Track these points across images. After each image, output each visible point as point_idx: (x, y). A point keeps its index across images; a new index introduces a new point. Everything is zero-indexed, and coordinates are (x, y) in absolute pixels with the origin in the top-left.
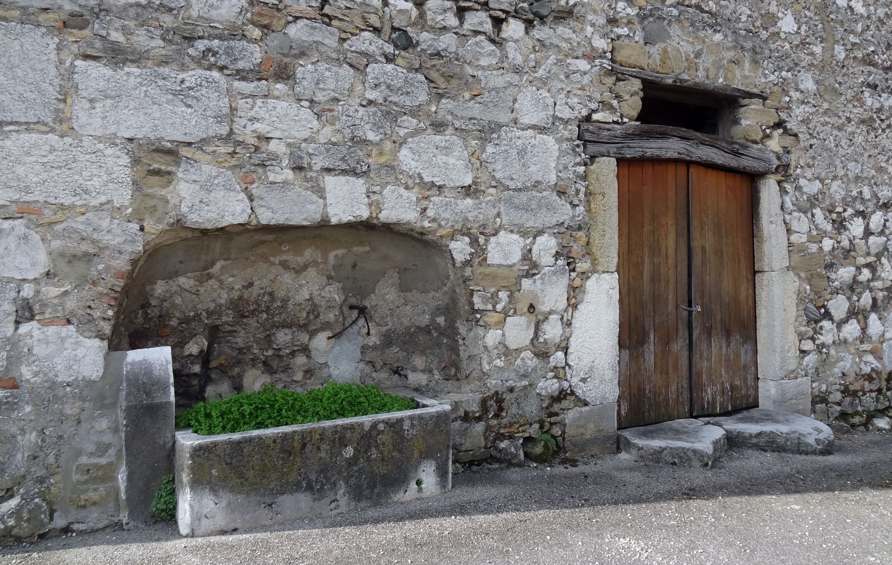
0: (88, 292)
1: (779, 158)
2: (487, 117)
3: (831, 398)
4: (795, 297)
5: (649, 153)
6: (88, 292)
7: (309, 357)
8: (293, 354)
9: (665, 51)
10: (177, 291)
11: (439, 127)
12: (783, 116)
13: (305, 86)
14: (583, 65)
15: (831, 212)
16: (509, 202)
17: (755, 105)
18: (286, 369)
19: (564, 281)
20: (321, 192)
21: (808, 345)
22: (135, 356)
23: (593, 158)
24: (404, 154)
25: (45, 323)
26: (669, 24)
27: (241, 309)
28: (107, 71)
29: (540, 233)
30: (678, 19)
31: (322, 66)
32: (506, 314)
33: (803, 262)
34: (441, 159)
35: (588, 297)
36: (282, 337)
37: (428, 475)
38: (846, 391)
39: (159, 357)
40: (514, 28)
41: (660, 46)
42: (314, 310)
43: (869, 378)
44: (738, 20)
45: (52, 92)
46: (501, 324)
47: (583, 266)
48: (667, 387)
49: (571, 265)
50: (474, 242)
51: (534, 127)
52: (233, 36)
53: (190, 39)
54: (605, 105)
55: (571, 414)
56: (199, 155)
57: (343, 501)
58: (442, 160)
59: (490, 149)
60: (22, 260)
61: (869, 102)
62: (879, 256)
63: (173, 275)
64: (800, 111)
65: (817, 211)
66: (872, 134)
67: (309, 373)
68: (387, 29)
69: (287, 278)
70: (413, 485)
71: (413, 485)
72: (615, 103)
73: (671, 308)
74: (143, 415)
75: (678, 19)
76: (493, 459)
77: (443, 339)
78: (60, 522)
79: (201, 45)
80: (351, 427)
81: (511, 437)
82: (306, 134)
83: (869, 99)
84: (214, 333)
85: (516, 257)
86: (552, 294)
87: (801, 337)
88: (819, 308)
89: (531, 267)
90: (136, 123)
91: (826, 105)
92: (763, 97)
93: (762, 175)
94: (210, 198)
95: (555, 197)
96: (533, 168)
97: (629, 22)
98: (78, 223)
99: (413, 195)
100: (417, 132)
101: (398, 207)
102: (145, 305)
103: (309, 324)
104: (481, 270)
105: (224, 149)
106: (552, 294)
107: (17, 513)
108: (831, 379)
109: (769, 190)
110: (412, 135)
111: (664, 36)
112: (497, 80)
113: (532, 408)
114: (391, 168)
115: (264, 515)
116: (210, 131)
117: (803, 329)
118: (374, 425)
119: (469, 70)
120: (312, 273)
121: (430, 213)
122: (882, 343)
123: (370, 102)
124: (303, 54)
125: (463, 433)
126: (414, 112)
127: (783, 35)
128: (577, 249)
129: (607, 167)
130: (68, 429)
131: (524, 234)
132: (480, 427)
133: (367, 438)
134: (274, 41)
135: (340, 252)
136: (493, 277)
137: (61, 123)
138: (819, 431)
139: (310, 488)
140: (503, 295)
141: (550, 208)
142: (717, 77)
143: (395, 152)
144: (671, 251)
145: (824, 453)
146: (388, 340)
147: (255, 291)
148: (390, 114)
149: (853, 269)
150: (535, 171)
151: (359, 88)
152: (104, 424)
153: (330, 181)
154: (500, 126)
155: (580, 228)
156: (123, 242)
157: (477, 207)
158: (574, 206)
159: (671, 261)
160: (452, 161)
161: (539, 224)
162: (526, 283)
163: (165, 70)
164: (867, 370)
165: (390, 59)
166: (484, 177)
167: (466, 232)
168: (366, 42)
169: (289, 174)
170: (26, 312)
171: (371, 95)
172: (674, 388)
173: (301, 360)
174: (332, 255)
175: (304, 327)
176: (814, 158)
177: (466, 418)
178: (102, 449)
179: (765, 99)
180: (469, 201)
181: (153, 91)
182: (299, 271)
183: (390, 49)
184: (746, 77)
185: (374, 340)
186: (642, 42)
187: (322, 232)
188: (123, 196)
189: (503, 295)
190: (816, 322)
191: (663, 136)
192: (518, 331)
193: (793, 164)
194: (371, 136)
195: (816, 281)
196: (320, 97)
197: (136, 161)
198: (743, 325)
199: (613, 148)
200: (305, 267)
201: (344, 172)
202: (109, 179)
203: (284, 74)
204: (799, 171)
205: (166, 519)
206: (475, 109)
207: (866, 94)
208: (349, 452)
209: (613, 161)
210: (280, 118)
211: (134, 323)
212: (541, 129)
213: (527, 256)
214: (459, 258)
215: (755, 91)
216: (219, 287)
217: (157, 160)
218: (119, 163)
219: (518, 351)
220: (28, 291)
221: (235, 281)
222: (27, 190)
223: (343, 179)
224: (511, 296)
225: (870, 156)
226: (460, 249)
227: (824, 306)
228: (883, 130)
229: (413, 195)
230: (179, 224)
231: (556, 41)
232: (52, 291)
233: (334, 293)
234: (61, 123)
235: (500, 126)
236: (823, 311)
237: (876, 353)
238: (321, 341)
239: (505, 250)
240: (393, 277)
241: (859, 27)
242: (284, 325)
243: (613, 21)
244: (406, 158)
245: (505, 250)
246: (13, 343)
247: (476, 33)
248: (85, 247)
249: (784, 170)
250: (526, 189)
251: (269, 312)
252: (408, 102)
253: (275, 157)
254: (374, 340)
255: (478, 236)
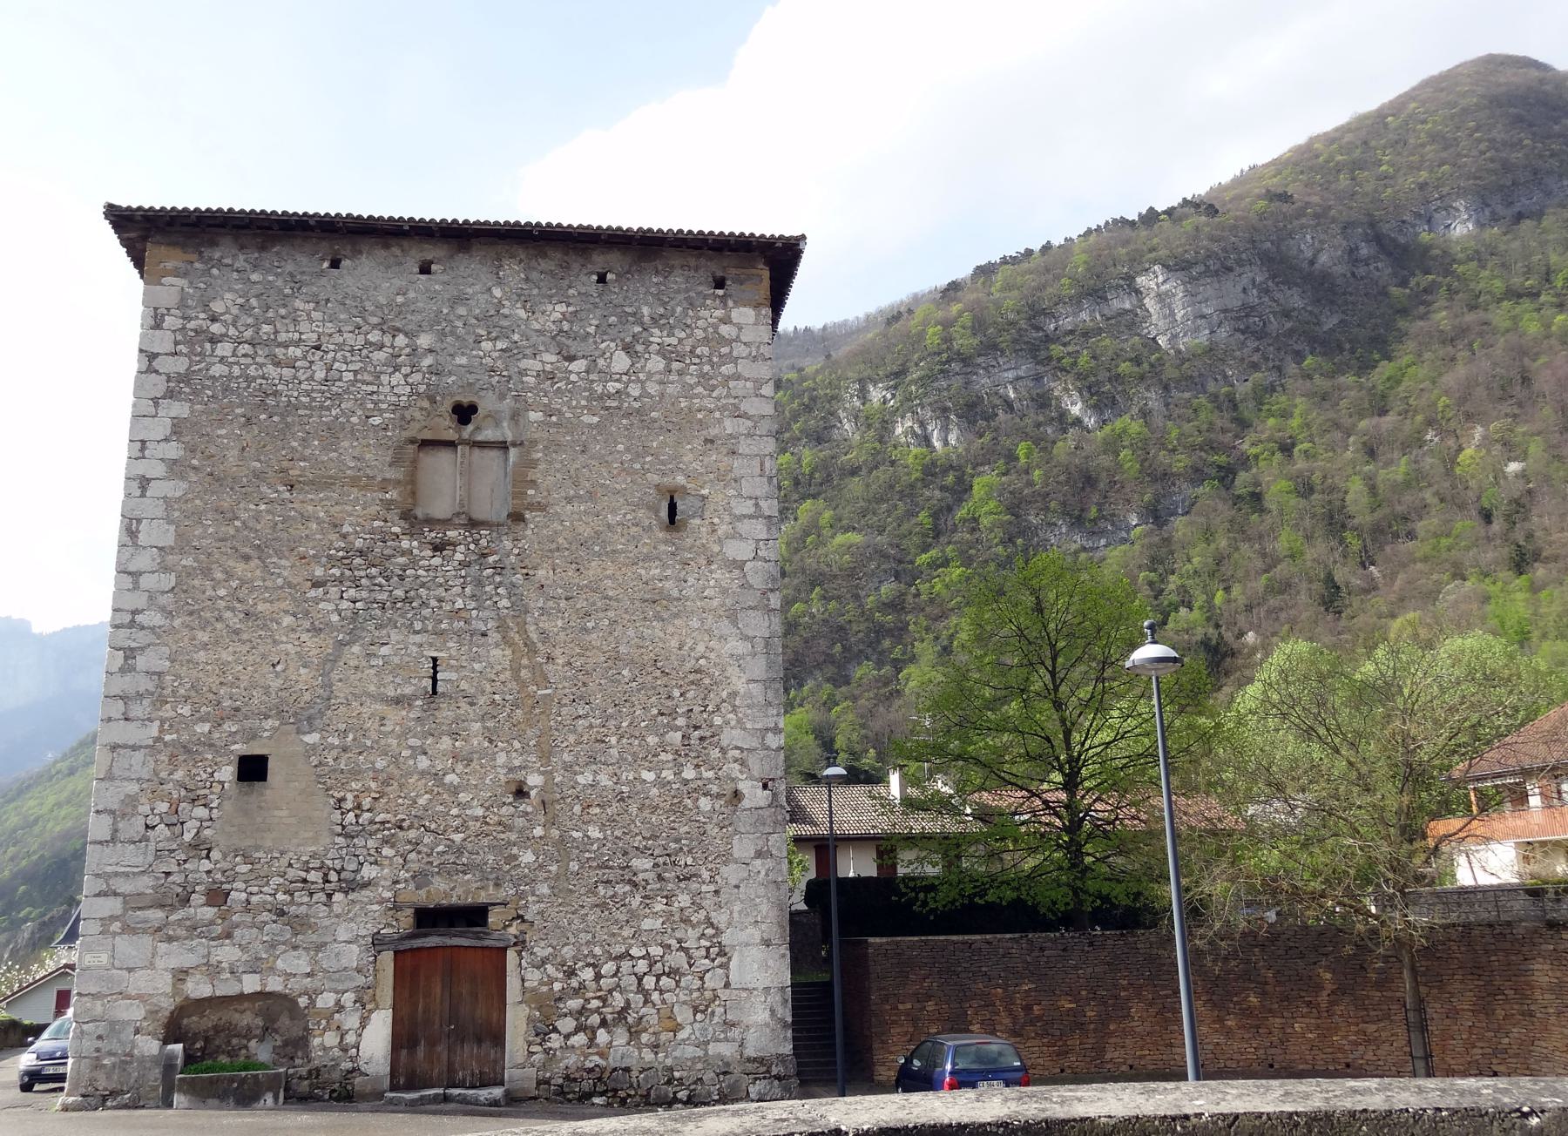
10: (192, 1022)
11: (295, 948)
17: (497, 909)
27: (217, 1029)
32: (325, 1030)
36: (235, 1041)
40: (338, 897)
42: (249, 1029)
43: (591, 1070)
46: (322, 1035)
47: (368, 1007)
49: (363, 1006)
54: (388, 925)
58: (299, 963)
64: (535, 908)
69: (237, 1015)
74: (168, 1067)
77: (300, 1043)
83: (601, 890)
84: (207, 1040)
85: (331, 1003)
89: (340, 1008)
90: (175, 963)
93: (505, 949)
94: (199, 988)
101: (275, 985)
106: (352, 1021)
109: (511, 955)
112: (327, 922)
113: (336, 1076)
114: (272, 968)
116: (752, 407)
129: (387, 958)
133: (243, 1081)
136: (318, 1014)
137: (152, 966)
141: (352, 979)
146: (286, 1044)
148: (273, 945)
150: (344, 962)
153: (245, 976)
156: (168, 1005)
162: (337, 1016)
164: (589, 1065)
167: (306, 993)
168: (266, 916)
170: (137, 1031)
173: (244, 1051)
175: (245, 1037)
177: (300, 1078)
182: (243, 1012)
187: (241, 997)
188: (169, 990)
191: (426, 935)
192: (331, 1039)
202: (164, 983)
203: (229, 936)
205: (170, 1106)
206: (314, 937)
210: (227, 953)
211: (173, 1031)
213: (338, 1002)
217: (181, 975)
218: (168, 977)
221: (215, 1018)
226: (303, 1001)
230: (187, 998)
233: (259, 1022)
234: (152, 966)
237: (602, 1055)
238: (253, 1043)
239: (326, 1001)
240: (286, 1013)
243: (396, 882)
244: (280, 964)
245: (326, 1001)
246: (133, 1042)
249: (520, 943)
251: (228, 1030)
254: (279, 1043)
255: (312, 994)
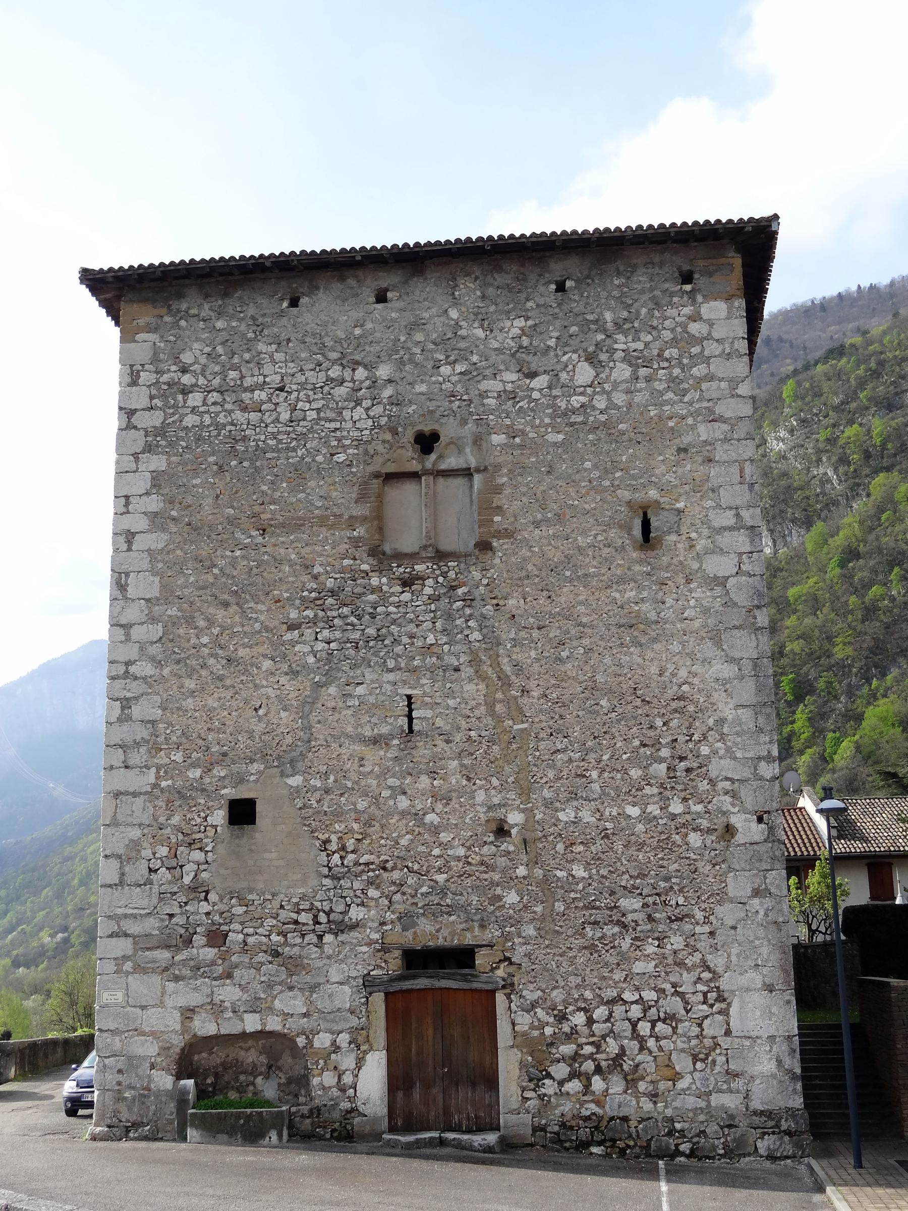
0: (168, 1060)
1: (504, 980)
2: (314, 981)
3: (549, 1129)
4: (517, 1064)
5: (405, 988)
6: (168, 1060)
7: (255, 1087)
8: (248, 1085)
9: (415, 933)
10: (201, 1058)
11: (291, 988)
12: (508, 955)
13: (237, 979)
14: (365, 949)
15: (553, 1010)
16: (325, 1019)
17: (484, 951)
18: (245, 1092)
19: (354, 1055)
20: (242, 1020)
21: (528, 1094)
22: (182, 1082)
23: (370, 993)
24: (277, 1002)
25: (157, 1070)
26: (418, 917)
27: (225, 1066)
28: (174, 985)
29: (341, 1032)
30: (423, 914)
31: (243, 970)
32: (323, 1070)
33: (522, 1040)
34: (293, 1002)
35: (367, 1063)
36: (242, 1078)
37: (274, 1135)
38: (563, 1125)
39: (190, 1083)
41: (412, 931)
42: (255, 1066)
43: (587, 1119)
44: (470, 905)
45: (160, 994)
46: (320, 1075)
47: (363, 1048)
48: (428, 1113)
50: (307, 1038)
51: (337, 983)
52: (212, 965)
53: (199, 969)
54: (378, 967)
55: (357, 1120)
56: (201, 1010)
57: (240, 1140)
58: (294, 1003)
59: (315, 996)
60: (151, 1050)
61: (590, 934)
62: (604, 1037)
63: (200, 1053)
64: (522, 950)
65: (538, 1010)
66: (596, 955)
67: (255, 1094)
68: (269, 951)
69: (242, 1053)
70: (268, 1139)
71: (268, 1139)
72: (383, 965)
73: (430, 1069)
75: (423, 914)
76: (314, 1136)
78: (160, 1136)
79: (202, 970)
80: (243, 1112)
81: (325, 1127)
82: (237, 998)
84: (216, 1075)
85: (328, 1044)
86: (347, 1062)
87: (524, 1089)
88: (541, 1072)
89: (336, 1048)
90: (182, 1001)
91: (547, 942)
92: (491, 946)
94: (205, 1026)
95: (349, 1014)
96: (337, 1002)
97: (392, 922)
98: (166, 1037)
99: (280, 1019)
100: (282, 992)
101: (274, 1024)
102: (192, 1064)
103: (254, 1071)
104: (312, 1050)
105: (209, 1007)
106: (347, 1062)
107: (149, 1130)
108: (552, 1117)
109: (500, 997)
110: (279, 993)
111: (415, 924)
112: (319, 963)
113: (336, 1115)
114: (270, 1008)
115: (212, 1139)
117: (524, 1084)
118: (252, 1112)
119: (306, 961)
120: (253, 1050)
121: (287, 1026)
122: (606, 1096)
123: (262, 982)
124: (236, 967)
125: (301, 1123)
126: (280, 984)
127: (507, 906)
128: (360, 1039)
129: (378, 999)
130: (163, 1106)
131: (333, 1033)
132: (308, 1121)
133: (249, 1117)
134: (227, 963)
135: (263, 1041)
136: (317, 1053)
137: (162, 1004)
138: (833, 1191)
139: (227, 1133)
140: (321, 1062)
141: (346, 1020)
142: (453, 940)
143: (272, 1002)
144: (430, 1038)
145: (484, 1151)
146: (290, 1081)
147: (230, 1058)
148: (270, 986)
149: (574, 1046)
150: (337, 1003)
151: (258, 977)
152: (172, 1105)
153: (246, 1016)
154: (320, 984)
155: (362, 1029)
156: (178, 1042)
157: (308, 1022)
158: (359, 1018)
159: (430, 1044)
160: (297, 1002)
161: (340, 1028)
162: (333, 1056)
163: (191, 981)
165: (270, 963)
166: (312, 1008)
169: (231, 1014)
170: (152, 1067)
171: (262, 979)
172: (433, 1114)
173: (251, 1088)
174: (260, 1043)
175: (251, 1074)
176: (535, 977)
178: (172, 1114)
179: (492, 947)
180: (305, 1019)
181: (187, 989)
182: (248, 1049)
183: (270, 958)
184: (476, 937)
185: (283, 1081)
186: (400, 930)
187: (244, 1035)
188: (178, 1027)
189: (321, 1062)
190: (539, 1080)
191: (414, 977)
193: (516, 982)
194: (263, 996)
195: (537, 1054)
196: (243, 983)
197: (182, 1014)
198: (492, 1083)
199: (382, 988)
200: (249, 1048)
201: (251, 1012)
202: (173, 1021)
203: (229, 976)
204: (521, 987)
205: (184, 1139)
206: (308, 978)
207: (588, 929)
208: (242, 1121)
209: (383, 994)
210: (228, 993)
212: (341, 983)
213: (334, 1042)
214: (300, 1045)
215: (484, 943)
216: (218, 1057)
217: (188, 1013)
218: (177, 1015)
219: (330, 1088)
220: (153, 1060)
221: (222, 1055)
222: (153, 1027)
223: (251, 1014)
224: (325, 1062)
225: (592, 970)
226: (301, 1041)
227: (546, 1070)
228: (607, 951)
229: (280, 1019)
230: (195, 1035)
231: (349, 940)
232: (159, 1060)
233: (263, 1059)
234: (162, 1004)
235: (320, 984)
236: (544, 1073)
238: (259, 1080)
239: (322, 1041)
241: (580, 887)
242: (242, 1073)
243: (383, 924)
244: (277, 1004)
245: (322, 1041)
246: (149, 1076)
247: (309, 944)
248: (168, 1045)
250: (333, 1012)
251: (236, 1067)
252: (278, 980)
253: (226, 1008)
254: (283, 1081)
255: (309, 1034)
